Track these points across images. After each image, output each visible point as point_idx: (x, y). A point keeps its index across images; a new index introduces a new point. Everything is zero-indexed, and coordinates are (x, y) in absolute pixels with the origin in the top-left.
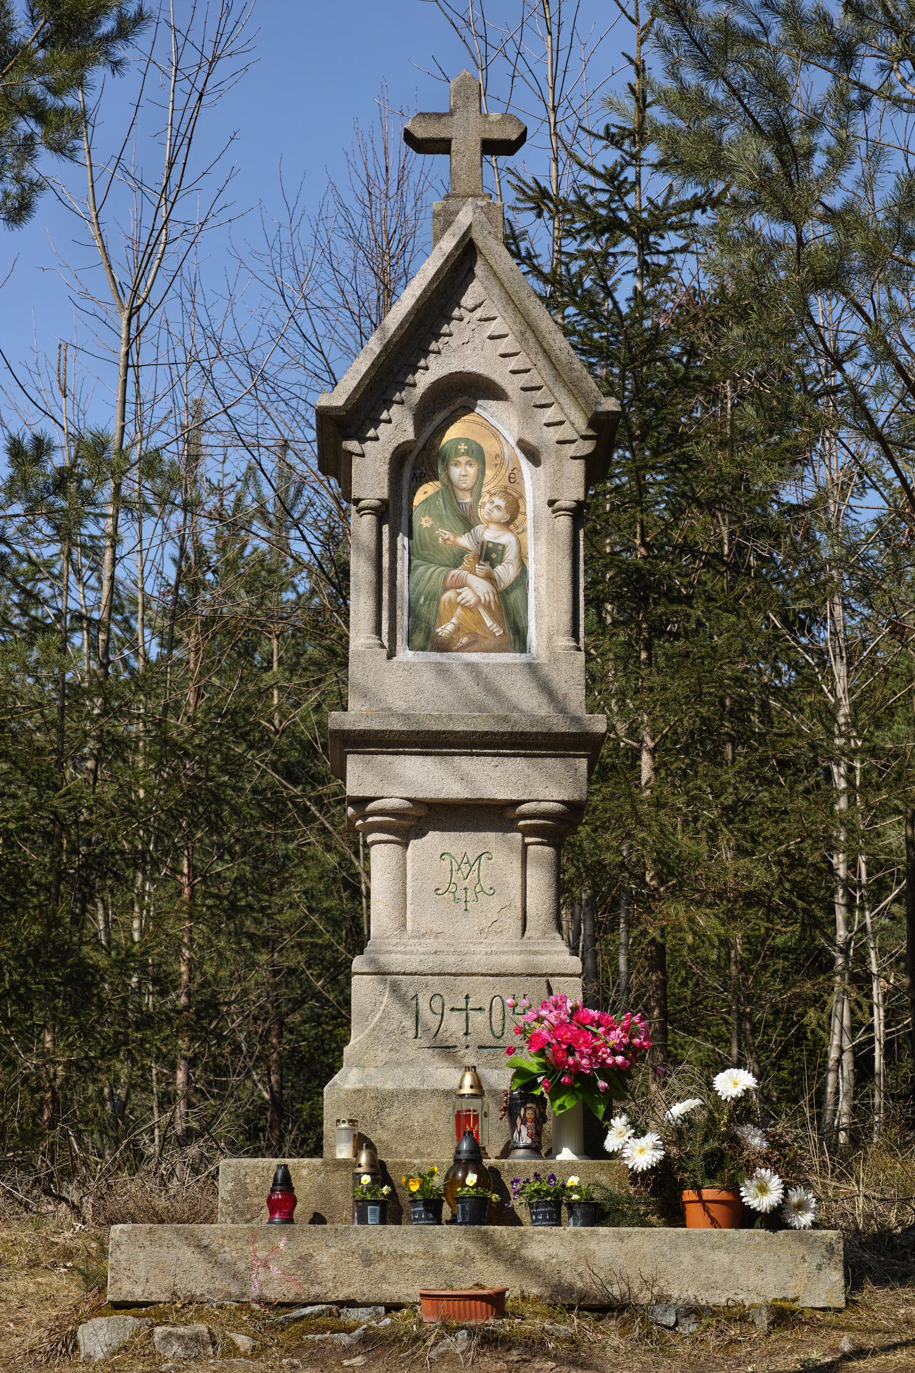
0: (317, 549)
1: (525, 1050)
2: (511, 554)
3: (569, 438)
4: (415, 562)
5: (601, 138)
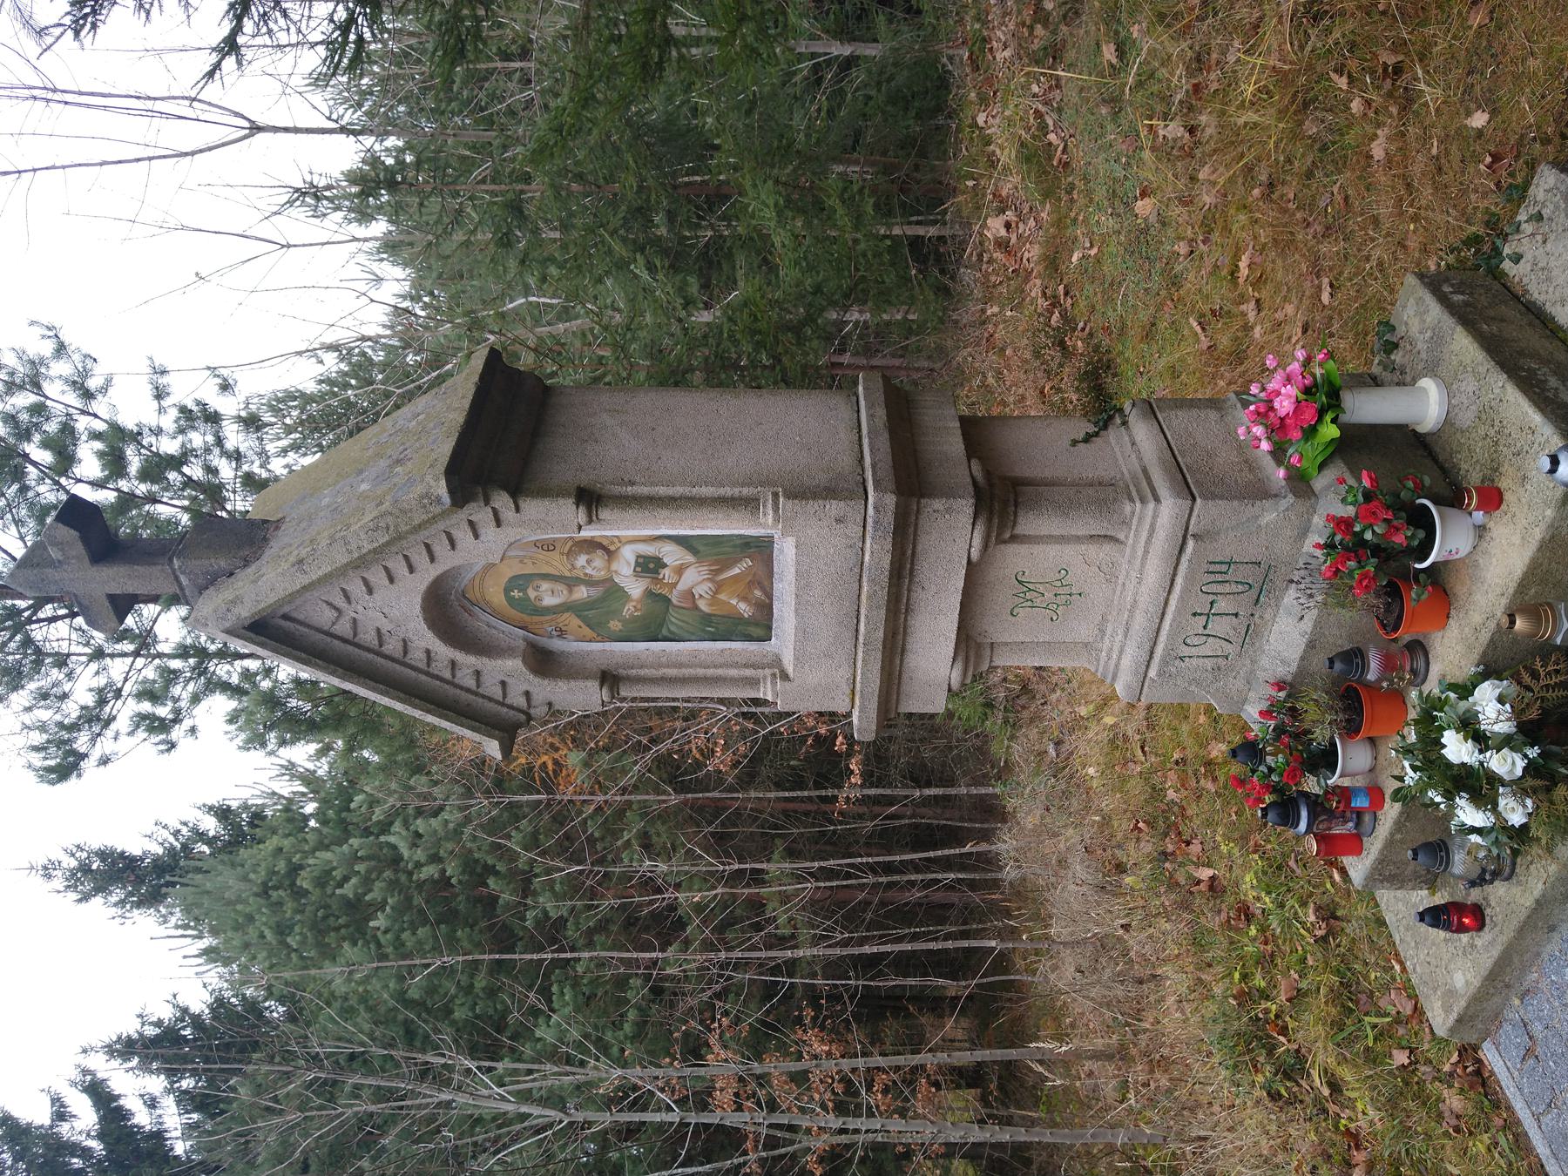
1: (1211, 1008)
2: (648, 550)
3: (491, 515)
4: (665, 632)
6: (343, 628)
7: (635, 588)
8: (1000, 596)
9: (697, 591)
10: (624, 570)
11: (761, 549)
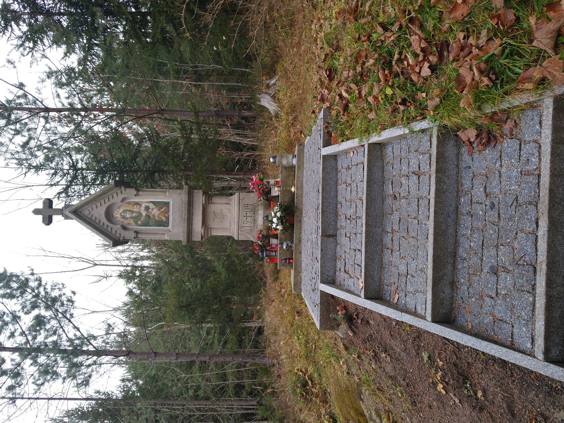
0: (145, 253)
2: (147, 204)
5: (33, 54)
6: (90, 216)
7: (144, 214)
8: (211, 216)
9: (156, 215)
10: (143, 208)
11: (167, 204)
